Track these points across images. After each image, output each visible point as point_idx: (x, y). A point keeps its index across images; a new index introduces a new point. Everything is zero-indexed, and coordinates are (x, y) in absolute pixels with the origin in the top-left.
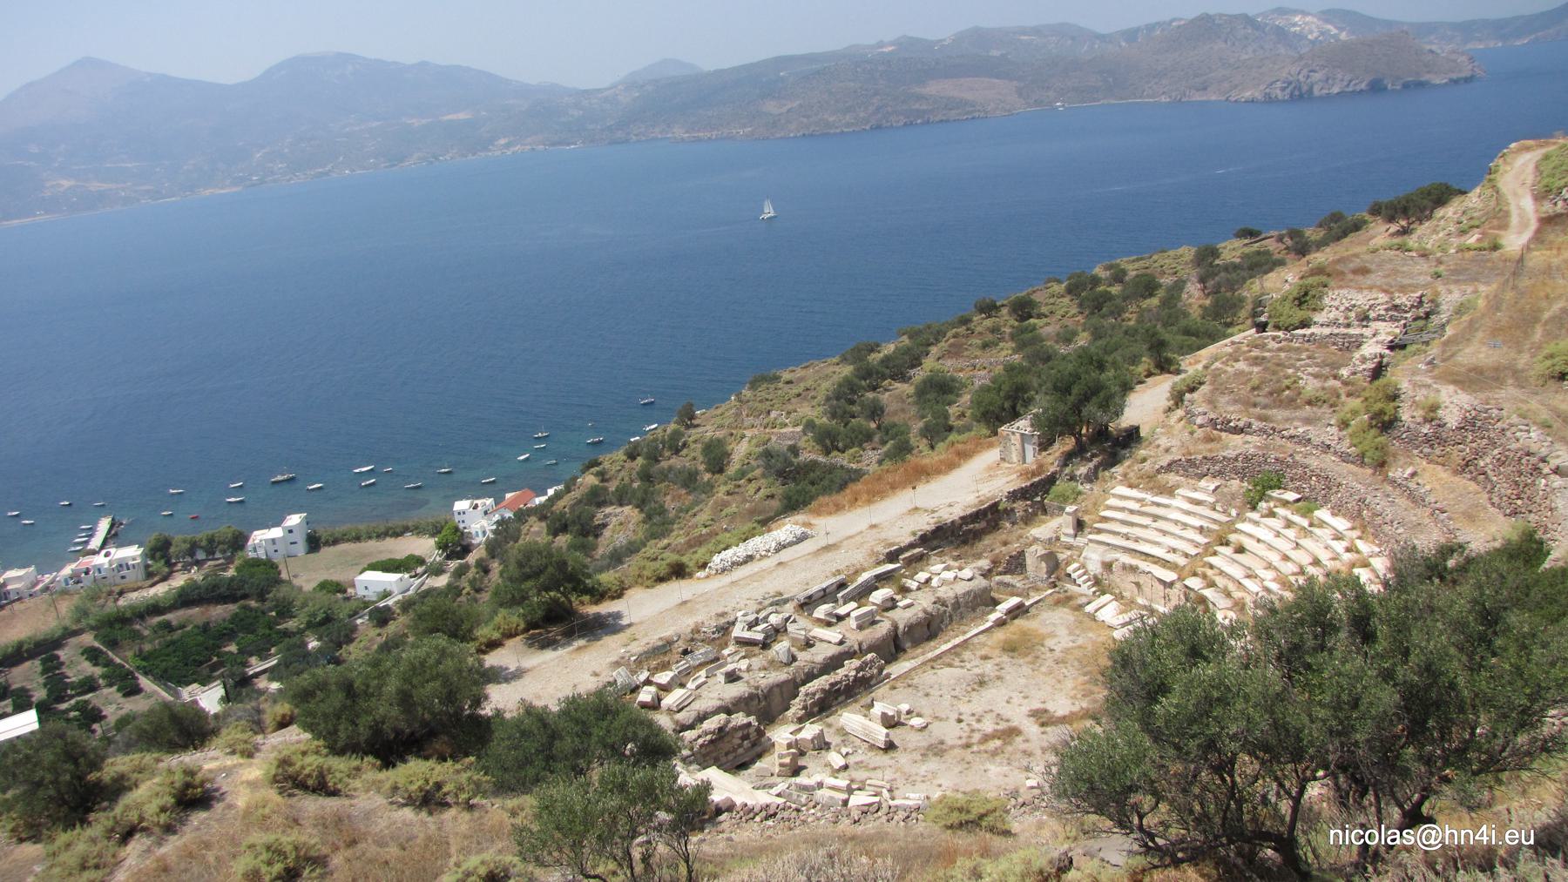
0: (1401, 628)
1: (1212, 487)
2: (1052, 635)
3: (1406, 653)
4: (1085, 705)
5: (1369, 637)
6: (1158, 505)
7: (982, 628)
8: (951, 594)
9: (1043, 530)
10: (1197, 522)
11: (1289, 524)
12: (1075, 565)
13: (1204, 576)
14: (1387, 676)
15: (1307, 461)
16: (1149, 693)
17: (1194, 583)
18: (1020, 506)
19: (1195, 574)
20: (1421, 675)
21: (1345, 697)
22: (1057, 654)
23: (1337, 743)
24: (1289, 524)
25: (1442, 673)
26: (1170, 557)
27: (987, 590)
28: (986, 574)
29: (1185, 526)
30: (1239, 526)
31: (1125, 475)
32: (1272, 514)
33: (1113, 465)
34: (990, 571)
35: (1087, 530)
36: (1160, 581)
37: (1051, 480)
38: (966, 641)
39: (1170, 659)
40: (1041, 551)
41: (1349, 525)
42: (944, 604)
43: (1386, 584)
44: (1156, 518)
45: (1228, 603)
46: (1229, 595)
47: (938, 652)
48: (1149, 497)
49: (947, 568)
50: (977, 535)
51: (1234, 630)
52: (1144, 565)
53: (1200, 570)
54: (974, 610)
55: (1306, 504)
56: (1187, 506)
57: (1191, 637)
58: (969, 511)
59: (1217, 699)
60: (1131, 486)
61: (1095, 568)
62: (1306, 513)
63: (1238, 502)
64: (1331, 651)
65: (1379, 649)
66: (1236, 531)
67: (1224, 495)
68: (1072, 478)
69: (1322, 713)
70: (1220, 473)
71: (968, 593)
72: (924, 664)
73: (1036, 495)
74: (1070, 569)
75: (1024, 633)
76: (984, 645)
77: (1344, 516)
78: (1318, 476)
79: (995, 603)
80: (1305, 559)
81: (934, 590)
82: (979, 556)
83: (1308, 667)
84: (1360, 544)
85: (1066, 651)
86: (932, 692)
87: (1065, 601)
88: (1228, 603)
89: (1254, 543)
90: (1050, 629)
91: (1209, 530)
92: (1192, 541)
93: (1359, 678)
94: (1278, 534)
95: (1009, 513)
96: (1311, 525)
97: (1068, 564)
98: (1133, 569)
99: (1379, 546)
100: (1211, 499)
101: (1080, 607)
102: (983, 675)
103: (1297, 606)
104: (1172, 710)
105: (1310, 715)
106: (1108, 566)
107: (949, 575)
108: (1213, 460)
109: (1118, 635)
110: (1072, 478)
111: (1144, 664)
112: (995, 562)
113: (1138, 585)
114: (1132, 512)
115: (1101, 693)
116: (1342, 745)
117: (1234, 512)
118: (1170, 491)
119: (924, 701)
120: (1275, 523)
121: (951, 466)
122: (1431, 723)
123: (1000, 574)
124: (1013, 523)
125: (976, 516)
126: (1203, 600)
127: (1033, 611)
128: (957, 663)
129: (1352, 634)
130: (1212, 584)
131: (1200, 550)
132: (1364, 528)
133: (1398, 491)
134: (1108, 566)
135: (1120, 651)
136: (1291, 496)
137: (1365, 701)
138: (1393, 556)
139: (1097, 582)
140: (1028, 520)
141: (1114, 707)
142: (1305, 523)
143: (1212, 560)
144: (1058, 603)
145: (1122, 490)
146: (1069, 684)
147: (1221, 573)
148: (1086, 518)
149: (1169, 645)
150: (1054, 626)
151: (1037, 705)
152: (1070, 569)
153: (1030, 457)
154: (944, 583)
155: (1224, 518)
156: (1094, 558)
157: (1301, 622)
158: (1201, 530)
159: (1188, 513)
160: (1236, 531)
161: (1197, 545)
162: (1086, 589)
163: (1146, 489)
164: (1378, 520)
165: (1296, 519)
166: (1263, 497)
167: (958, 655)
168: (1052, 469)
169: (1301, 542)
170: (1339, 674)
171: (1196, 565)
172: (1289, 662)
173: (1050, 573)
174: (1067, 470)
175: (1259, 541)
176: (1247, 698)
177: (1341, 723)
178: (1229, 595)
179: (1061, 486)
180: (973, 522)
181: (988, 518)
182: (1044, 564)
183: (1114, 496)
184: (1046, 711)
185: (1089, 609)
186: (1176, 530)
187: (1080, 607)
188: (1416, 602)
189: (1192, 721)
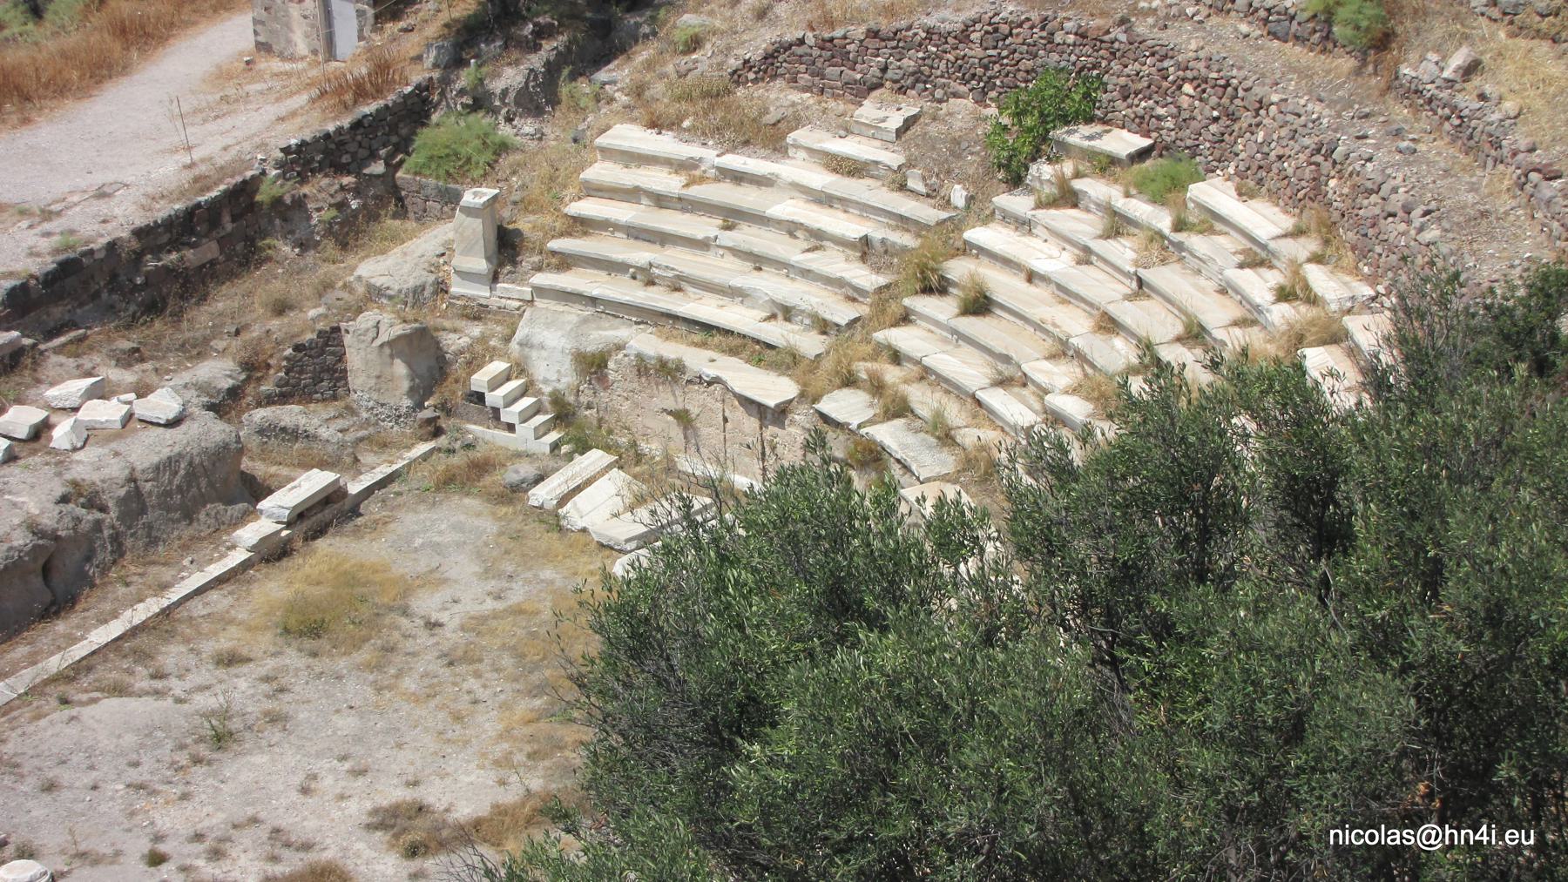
0: (1417, 508)
1: (896, 121)
2: (433, 579)
3: (1433, 578)
4: (536, 784)
5: (1331, 537)
6: (738, 177)
7: (215, 570)
8: (115, 470)
9: (395, 263)
10: (850, 227)
11: (1117, 225)
12: (497, 367)
13: (877, 387)
14: (1382, 644)
15: (1168, 37)
16: (713, 728)
17: (847, 406)
18: (321, 191)
19: (849, 381)
20: (1475, 639)
21: (1266, 712)
22: (452, 636)
23: (1247, 843)
24: (1117, 225)
25: (1532, 630)
26: (776, 332)
27: (228, 454)
28: (225, 404)
29: (818, 239)
30: (977, 234)
31: (638, 91)
32: (1068, 197)
33: (602, 59)
34: (234, 393)
35: (528, 260)
36: (748, 403)
37: (417, 109)
38: (166, 612)
39: (774, 619)
40: (391, 327)
41: (1288, 222)
42: (93, 501)
43: (1376, 380)
44: (732, 217)
45: (947, 462)
46: (946, 437)
47: (79, 651)
48: (710, 155)
49: (101, 392)
50: (196, 284)
51: (952, 535)
52: (699, 360)
53: (862, 369)
54: (189, 516)
55: (1166, 165)
56: (820, 179)
57: (828, 557)
58: (163, 211)
59: (905, 740)
60: (655, 124)
61: (554, 370)
62: (1168, 191)
63: (971, 163)
64: (1225, 581)
65: (1359, 567)
66: (968, 249)
67: (930, 143)
68: (480, 102)
69: (1205, 760)
70: (919, 79)
71: (170, 464)
72: (36, 690)
73: (369, 156)
74: (480, 380)
75: (351, 580)
76: (225, 621)
77: (1274, 196)
78: (1200, 81)
79: (256, 490)
80: (1158, 324)
81: (61, 459)
82: (198, 350)
83: (1163, 628)
84: (1319, 279)
85: (476, 625)
86: (65, 775)
87: (473, 474)
88: (947, 462)
89: (1019, 283)
90: (423, 564)
91: (888, 249)
92: (839, 283)
93: (1301, 656)
94: (1086, 257)
95: (289, 212)
96: (1179, 226)
97: (474, 364)
98: (669, 371)
99: (1372, 280)
100: (892, 158)
101: (516, 491)
102: (225, 714)
103: (1115, 462)
104: (780, 776)
105: (1171, 768)
106: (593, 366)
107: (108, 412)
108: (897, 41)
109: (619, 568)
110: (480, 102)
111: (697, 646)
112: (253, 367)
113: (683, 418)
114: (661, 201)
115: (577, 736)
116: (1262, 847)
117: (958, 195)
118: (773, 138)
119: (40, 808)
120: (1080, 224)
121: (98, 71)
122: (1505, 771)
123: (269, 400)
124: (304, 245)
125: (186, 225)
126: (873, 456)
127: (372, 509)
128: (142, 682)
129: (1284, 532)
130: (899, 409)
131: (862, 310)
132: (1328, 233)
133: (1425, 121)
134: (593, 366)
135: (624, 611)
136: (1123, 142)
137: (1321, 716)
138: (1407, 312)
139: (563, 414)
140: (349, 232)
141: (614, 781)
142: (1163, 221)
143: (900, 337)
144: (448, 482)
145: (630, 135)
146: (488, 723)
147: (926, 374)
148: (524, 224)
149: (766, 586)
150: (438, 551)
151: (394, 793)
152: (480, 380)
153: (348, 40)
154: (90, 435)
155: (928, 213)
156: (551, 343)
157: (1140, 502)
158: (864, 248)
159: (825, 200)
160: (968, 249)
161: (853, 294)
162: (529, 437)
163: (702, 133)
164: (1371, 206)
165: (1139, 209)
166: (1041, 145)
167: (143, 656)
168: (417, 76)
169: (1145, 274)
170: (1250, 646)
171: (852, 353)
172: (1111, 618)
173: (420, 393)
174: (464, 78)
175: (1031, 276)
176: (993, 724)
177: (1258, 785)
178: (946, 437)
179: (446, 127)
180: (175, 244)
181: (224, 230)
182: (400, 368)
183: (609, 153)
184: (421, 809)
185: (542, 495)
186: (792, 251)
187: (516, 491)
188: (1458, 431)
189: (838, 804)
